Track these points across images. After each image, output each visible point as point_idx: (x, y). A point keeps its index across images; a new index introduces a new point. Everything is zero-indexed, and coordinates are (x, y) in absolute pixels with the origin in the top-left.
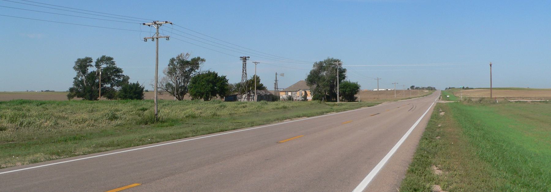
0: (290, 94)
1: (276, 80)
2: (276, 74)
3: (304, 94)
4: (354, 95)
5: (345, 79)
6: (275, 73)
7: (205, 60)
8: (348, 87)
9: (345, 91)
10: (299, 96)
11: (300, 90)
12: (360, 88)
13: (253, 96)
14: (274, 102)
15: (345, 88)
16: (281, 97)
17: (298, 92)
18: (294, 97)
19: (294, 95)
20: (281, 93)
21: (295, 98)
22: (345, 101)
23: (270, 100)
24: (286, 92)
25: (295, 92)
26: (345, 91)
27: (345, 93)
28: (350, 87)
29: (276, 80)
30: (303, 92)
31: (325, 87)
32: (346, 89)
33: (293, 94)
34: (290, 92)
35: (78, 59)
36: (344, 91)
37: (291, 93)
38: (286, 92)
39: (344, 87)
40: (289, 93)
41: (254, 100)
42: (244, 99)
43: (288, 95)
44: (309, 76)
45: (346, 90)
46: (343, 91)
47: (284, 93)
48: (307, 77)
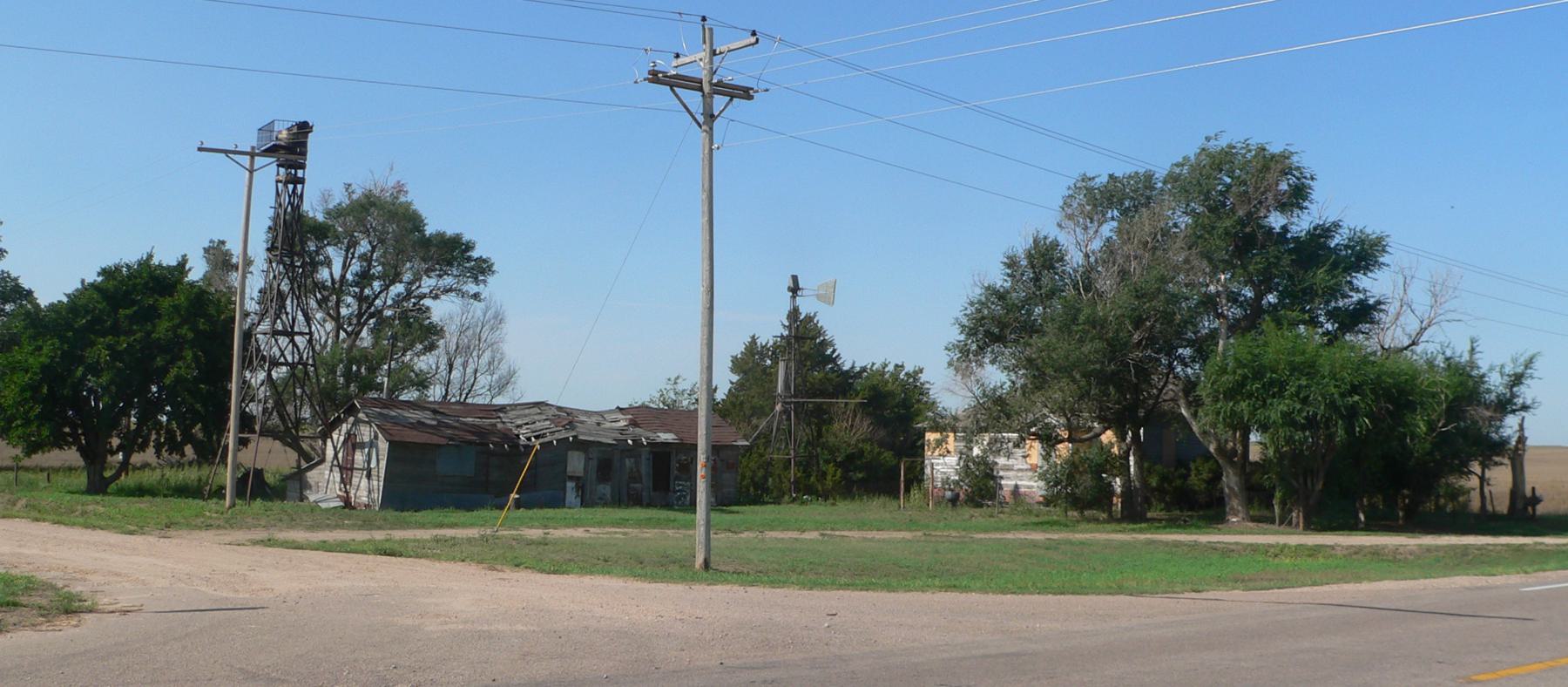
18: (1008, 468)
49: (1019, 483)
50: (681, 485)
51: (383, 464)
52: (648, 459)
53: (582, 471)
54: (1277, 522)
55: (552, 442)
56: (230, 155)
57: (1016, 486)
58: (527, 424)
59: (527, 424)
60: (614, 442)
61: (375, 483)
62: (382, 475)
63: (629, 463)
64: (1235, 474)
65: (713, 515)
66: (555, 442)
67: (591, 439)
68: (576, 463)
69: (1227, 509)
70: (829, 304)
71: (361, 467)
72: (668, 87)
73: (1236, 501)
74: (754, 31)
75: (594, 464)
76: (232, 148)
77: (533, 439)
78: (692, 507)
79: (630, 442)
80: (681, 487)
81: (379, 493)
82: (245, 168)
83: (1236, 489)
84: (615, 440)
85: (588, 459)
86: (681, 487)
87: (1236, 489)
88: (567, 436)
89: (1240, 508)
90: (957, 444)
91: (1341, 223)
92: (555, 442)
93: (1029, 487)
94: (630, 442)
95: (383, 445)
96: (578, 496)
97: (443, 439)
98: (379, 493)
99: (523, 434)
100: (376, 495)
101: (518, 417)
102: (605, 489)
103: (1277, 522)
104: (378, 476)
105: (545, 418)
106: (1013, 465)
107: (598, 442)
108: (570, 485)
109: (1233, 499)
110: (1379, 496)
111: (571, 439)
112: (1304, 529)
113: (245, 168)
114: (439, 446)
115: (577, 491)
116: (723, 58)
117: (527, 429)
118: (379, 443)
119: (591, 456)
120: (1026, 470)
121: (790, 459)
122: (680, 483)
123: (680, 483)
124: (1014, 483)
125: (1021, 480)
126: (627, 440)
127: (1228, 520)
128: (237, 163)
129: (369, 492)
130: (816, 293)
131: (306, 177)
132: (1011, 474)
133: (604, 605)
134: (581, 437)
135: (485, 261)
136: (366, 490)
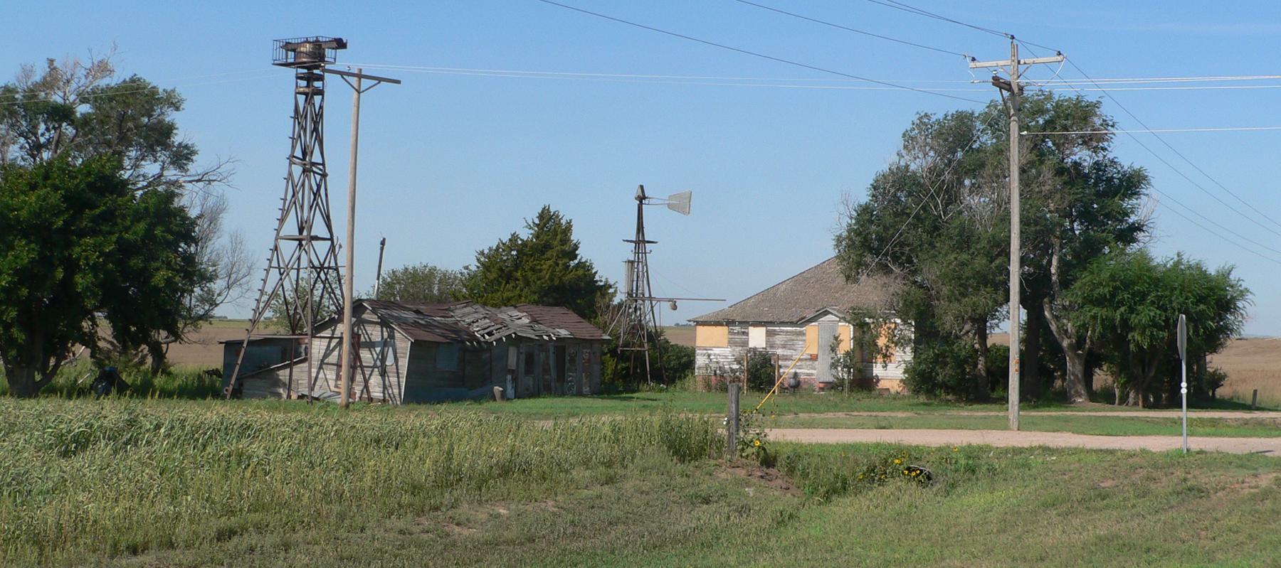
0: (757, 338)
1: (640, 241)
2: (642, 198)
3: (847, 344)
4: (1208, 358)
5: (1134, 240)
6: (636, 192)
7: (181, 101)
8: (1143, 296)
9: (1125, 322)
10: (814, 358)
11: (826, 313)
12: (1240, 304)
13: (385, 344)
14: (33, 401)
15: (1121, 303)
16: (700, 361)
17: (812, 330)
18: (787, 358)
19: (784, 346)
20: (699, 328)
21: (787, 371)
22: (1124, 400)
23: (571, 376)
24: (737, 329)
25: (792, 324)
26: (1125, 322)
27: (1121, 342)
28: (1159, 298)
29: (640, 241)
30: (847, 333)
31: (963, 295)
32: (1132, 310)
33: (778, 340)
34: (757, 324)
35: (569, 223)
36: (1114, 328)
37: (769, 334)
38: (730, 323)
39: (1113, 295)
40: (751, 330)
41: (383, 374)
42: (320, 368)
43: (745, 343)
44: (865, 211)
45: (1134, 320)
46: (1109, 325)
47: (723, 330)
48: (846, 221)
49: (798, 371)
50: (570, 376)
51: (404, 363)
52: (554, 353)
53: (515, 364)
54: (1117, 401)
55: (501, 338)
56: (344, 76)
57: (796, 375)
58: (473, 322)
59: (473, 322)
60: (537, 338)
61: (394, 380)
62: (404, 371)
63: (542, 355)
64: (1080, 364)
65: (1188, 413)
66: (504, 339)
67: (524, 335)
68: (513, 359)
69: (58, 372)
70: (684, 213)
71: (372, 365)
72: (998, 89)
73: (1080, 386)
74: (1059, 52)
75: (523, 357)
76: (346, 70)
77: (487, 337)
78: (1004, 400)
79: (545, 337)
80: (571, 378)
81: (400, 389)
82: (353, 87)
83: (1080, 375)
84: (537, 336)
85: (519, 353)
86: (571, 378)
87: (1080, 375)
88: (510, 333)
89: (1083, 392)
90: (730, 337)
91: (1115, 160)
92: (504, 339)
93: (808, 375)
94: (513, 335)
95: (404, 344)
96: (512, 387)
97: (442, 338)
98: (400, 389)
99: (477, 331)
100: (396, 391)
101: (464, 315)
102: (529, 381)
103: (1117, 401)
104: (398, 373)
105: (482, 316)
106: (792, 356)
107: (529, 338)
108: (509, 377)
109: (1078, 384)
110: (22, 341)
111: (513, 335)
112: (1144, 407)
113: (353, 87)
114: (439, 343)
115: (512, 383)
116: (1028, 68)
117: (477, 326)
118: (397, 342)
119: (521, 351)
120: (806, 359)
121: (644, 351)
122: (571, 374)
123: (571, 374)
124: (793, 371)
125: (800, 369)
126: (542, 336)
127: (1075, 400)
128: (349, 83)
129: (385, 387)
130: (666, 202)
131: (325, 90)
132: (789, 363)
133: (1177, 464)
134: (520, 334)
135: (186, 147)
136: (398, 383)
